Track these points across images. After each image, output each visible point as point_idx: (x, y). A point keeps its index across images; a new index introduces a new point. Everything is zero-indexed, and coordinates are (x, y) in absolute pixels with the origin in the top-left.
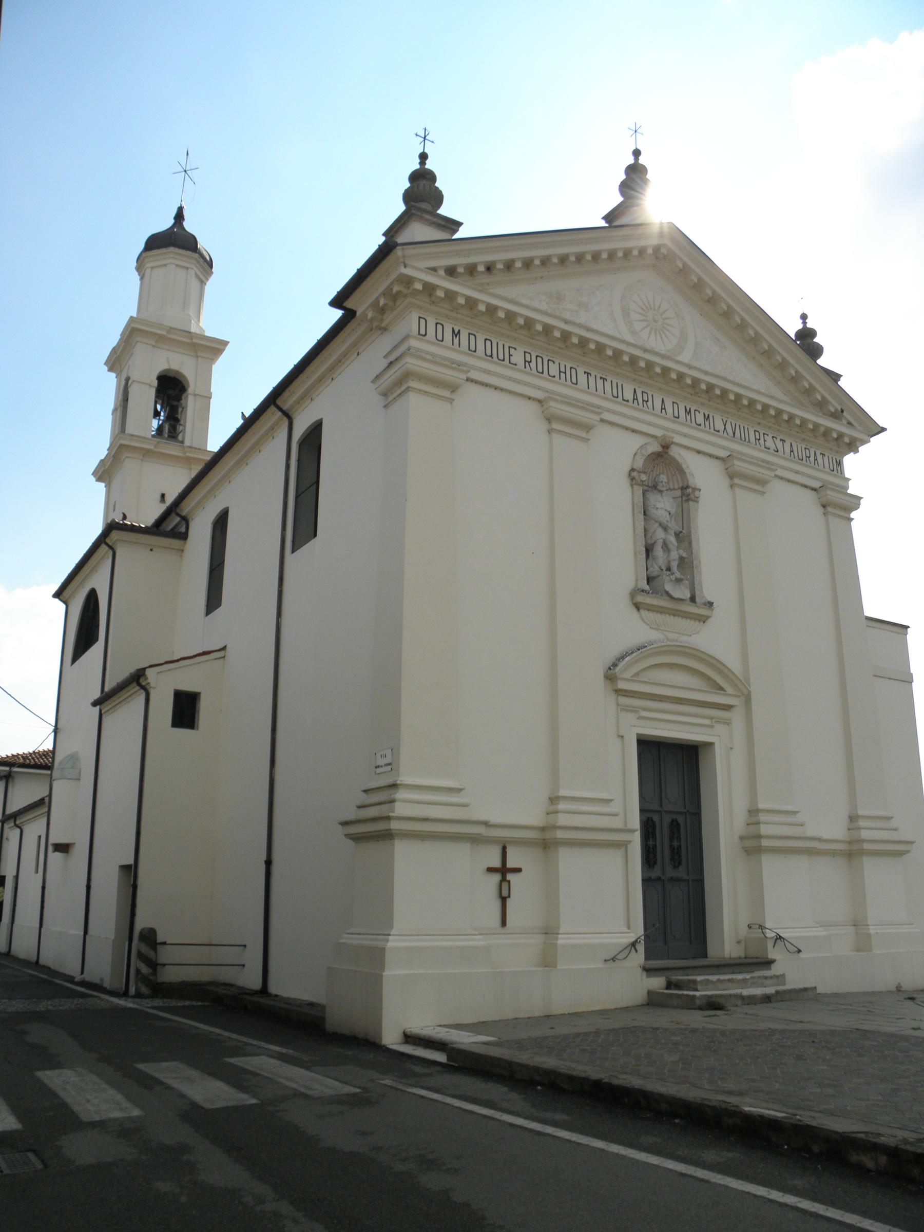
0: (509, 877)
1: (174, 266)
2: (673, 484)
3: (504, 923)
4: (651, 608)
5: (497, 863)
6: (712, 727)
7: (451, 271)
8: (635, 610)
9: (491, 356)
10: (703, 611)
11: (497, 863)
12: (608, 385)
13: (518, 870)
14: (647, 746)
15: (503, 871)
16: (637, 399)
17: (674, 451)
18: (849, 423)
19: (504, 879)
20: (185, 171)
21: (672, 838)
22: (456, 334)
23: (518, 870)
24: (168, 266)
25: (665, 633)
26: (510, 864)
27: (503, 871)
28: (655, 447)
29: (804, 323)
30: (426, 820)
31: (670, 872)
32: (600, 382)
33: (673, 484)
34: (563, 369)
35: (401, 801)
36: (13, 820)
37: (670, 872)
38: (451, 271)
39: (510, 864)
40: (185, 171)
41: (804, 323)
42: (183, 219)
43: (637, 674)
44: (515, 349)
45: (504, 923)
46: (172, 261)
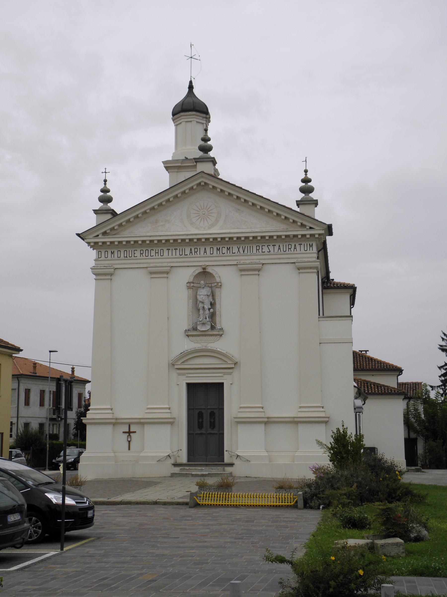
0: (131, 434)
1: (185, 122)
2: (210, 282)
3: (129, 449)
4: (193, 336)
5: (127, 430)
6: (222, 376)
7: (105, 233)
8: (187, 337)
9: (127, 257)
10: (221, 333)
11: (127, 430)
12: (178, 251)
13: (135, 432)
14: (189, 385)
15: (129, 433)
16: (192, 253)
17: (209, 270)
18: (311, 228)
19: (129, 435)
20: (191, 57)
21: (199, 419)
22: (112, 253)
23: (135, 432)
24: (182, 123)
25: (201, 343)
26: (131, 430)
27: (129, 433)
28: (200, 270)
29: (306, 174)
30: (93, 419)
31: (210, 431)
32: (174, 251)
33: (210, 282)
34: (157, 252)
35: (88, 414)
36: (399, 372)
37: (210, 431)
38: (105, 233)
39: (131, 430)
40: (191, 57)
41: (306, 174)
42: (193, 88)
43: (183, 362)
44: (137, 250)
45: (129, 449)
46: (183, 120)
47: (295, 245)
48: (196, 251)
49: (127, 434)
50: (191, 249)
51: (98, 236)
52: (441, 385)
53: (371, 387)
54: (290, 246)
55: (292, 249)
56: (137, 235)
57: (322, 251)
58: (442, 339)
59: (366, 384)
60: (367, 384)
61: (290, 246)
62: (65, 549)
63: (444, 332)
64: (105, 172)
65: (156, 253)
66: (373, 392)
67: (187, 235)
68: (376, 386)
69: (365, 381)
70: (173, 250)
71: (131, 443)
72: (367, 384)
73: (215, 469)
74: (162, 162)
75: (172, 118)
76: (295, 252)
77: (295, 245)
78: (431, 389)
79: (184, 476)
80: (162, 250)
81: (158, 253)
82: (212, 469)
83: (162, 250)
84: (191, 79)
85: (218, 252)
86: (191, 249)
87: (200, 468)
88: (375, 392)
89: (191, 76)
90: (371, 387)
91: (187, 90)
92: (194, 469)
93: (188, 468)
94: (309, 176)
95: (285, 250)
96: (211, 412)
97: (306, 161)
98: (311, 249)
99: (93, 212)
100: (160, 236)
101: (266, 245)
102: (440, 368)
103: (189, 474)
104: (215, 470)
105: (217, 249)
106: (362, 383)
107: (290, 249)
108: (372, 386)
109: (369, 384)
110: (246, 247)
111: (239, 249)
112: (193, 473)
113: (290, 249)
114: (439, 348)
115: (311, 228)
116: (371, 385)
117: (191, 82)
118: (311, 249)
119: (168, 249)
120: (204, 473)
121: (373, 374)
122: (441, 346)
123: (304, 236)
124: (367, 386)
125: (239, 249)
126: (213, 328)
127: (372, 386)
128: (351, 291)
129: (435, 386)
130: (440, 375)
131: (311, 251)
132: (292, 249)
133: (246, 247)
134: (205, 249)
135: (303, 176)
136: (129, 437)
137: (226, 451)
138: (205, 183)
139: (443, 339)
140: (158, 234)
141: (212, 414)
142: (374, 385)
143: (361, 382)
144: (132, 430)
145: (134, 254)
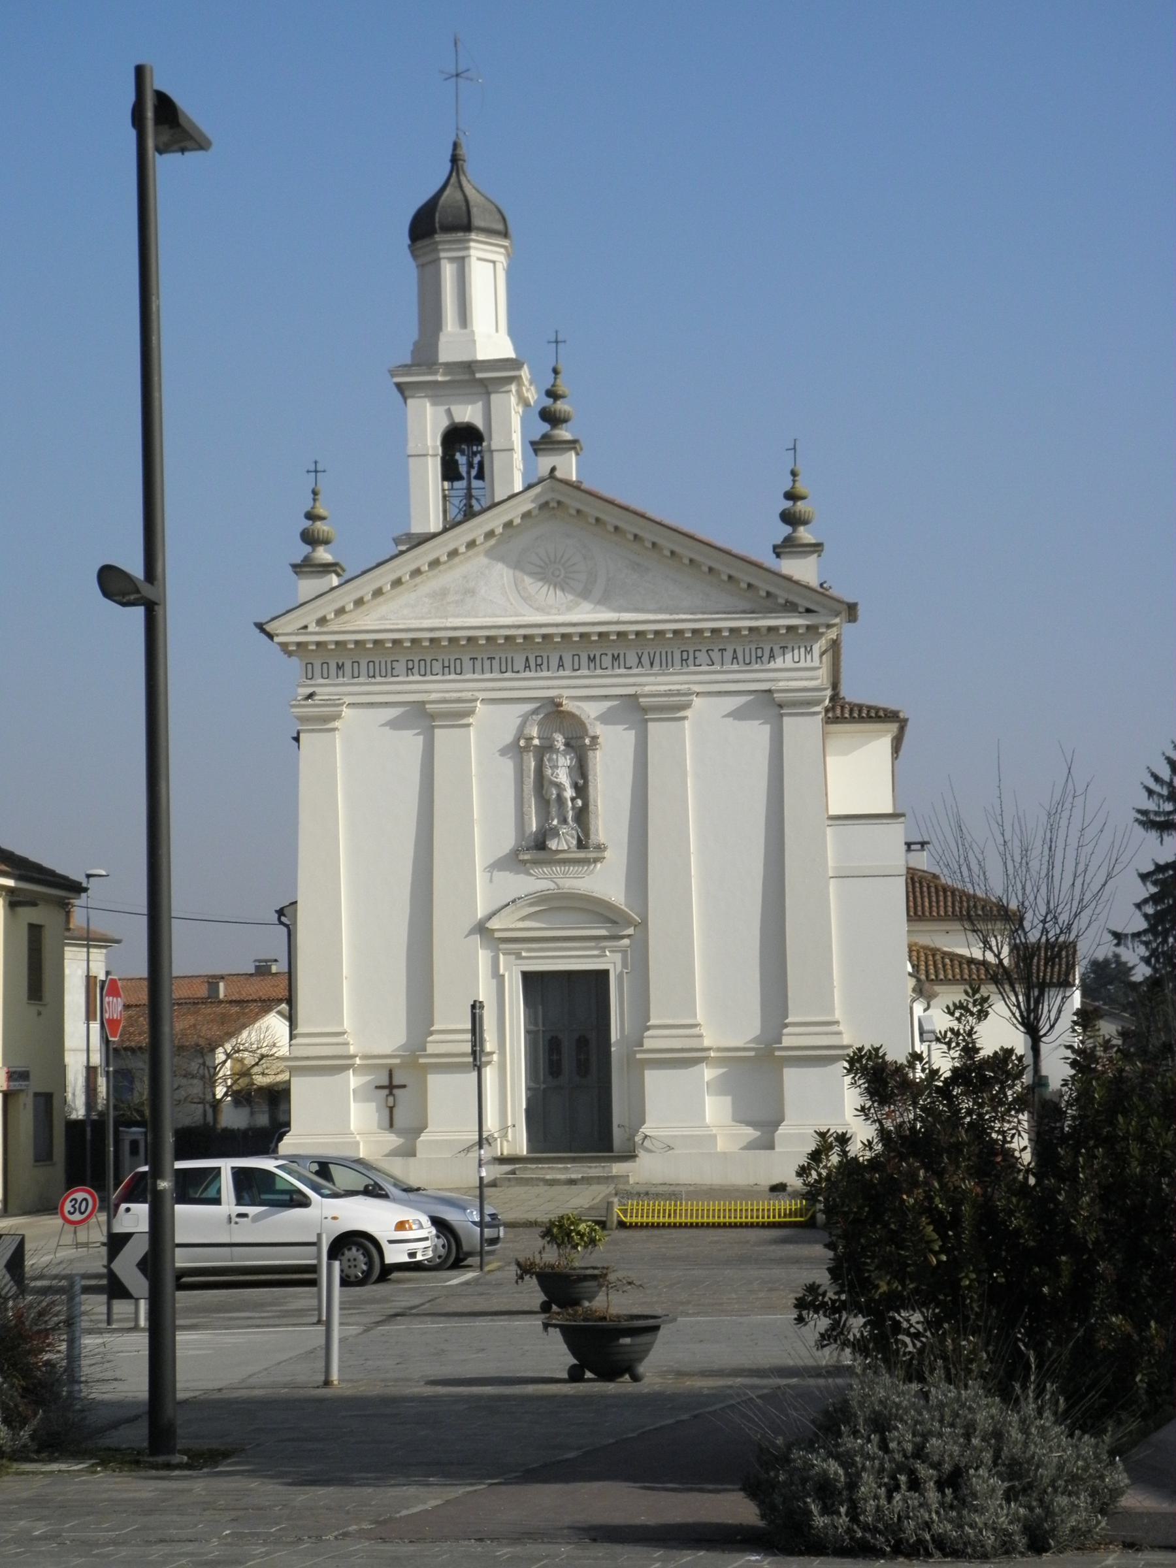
0: (396, 1091)
19: (391, 1094)
32: (487, 663)
34: (446, 664)
47: (772, 649)
48: (539, 662)
49: (386, 1092)
50: (527, 659)
51: (306, 627)
52: (1145, 932)
53: (944, 965)
54: (759, 651)
55: (765, 658)
56: (397, 624)
57: (830, 653)
58: (1146, 794)
59: (930, 958)
60: (934, 956)
61: (759, 651)
62: (487, 1269)
63: (1154, 770)
64: (316, 471)
65: (444, 667)
66: (950, 977)
67: (520, 627)
68: (956, 962)
69: (925, 948)
70: (485, 660)
71: (395, 1111)
72: (934, 956)
73: (596, 1167)
74: (201, 144)
75: (410, 246)
76: (772, 665)
77: (772, 649)
78: (1115, 942)
79: (527, 1185)
80: (458, 662)
81: (449, 667)
82: (590, 1167)
83: (458, 662)
84: (457, 135)
85: (592, 665)
86: (527, 659)
87: (560, 1166)
88: (954, 976)
89: (457, 129)
90: (944, 965)
91: (448, 165)
92: (549, 1168)
93: (534, 1166)
94: (801, 487)
95: (747, 661)
96: (553, 1037)
97: (795, 449)
98: (809, 657)
99: (290, 568)
100: (455, 629)
101: (704, 650)
102: (1144, 877)
103: (538, 1179)
104: (597, 1170)
105: (589, 657)
106: (922, 954)
107: (760, 658)
108: (947, 961)
109: (938, 957)
110: (658, 655)
111: (640, 659)
112: (548, 1177)
113: (760, 658)
114: (1137, 820)
115: (808, 611)
116: (943, 958)
117: (456, 146)
118: (809, 657)
119: (474, 659)
120: (574, 1176)
121: (948, 928)
122: (1144, 813)
123: (791, 629)
124: (935, 962)
125: (640, 659)
126: (581, 845)
127: (947, 961)
128: (894, 727)
129: (1126, 935)
130: (1138, 901)
131: (809, 664)
132: (765, 658)
133: (658, 655)
134: (561, 658)
135: (787, 486)
136: (391, 1099)
137: (619, 1126)
138: (559, 503)
139: (1150, 792)
140: (449, 625)
141: (582, 1043)
142: (951, 960)
143: (918, 952)
144: (396, 1082)
145: (393, 669)
